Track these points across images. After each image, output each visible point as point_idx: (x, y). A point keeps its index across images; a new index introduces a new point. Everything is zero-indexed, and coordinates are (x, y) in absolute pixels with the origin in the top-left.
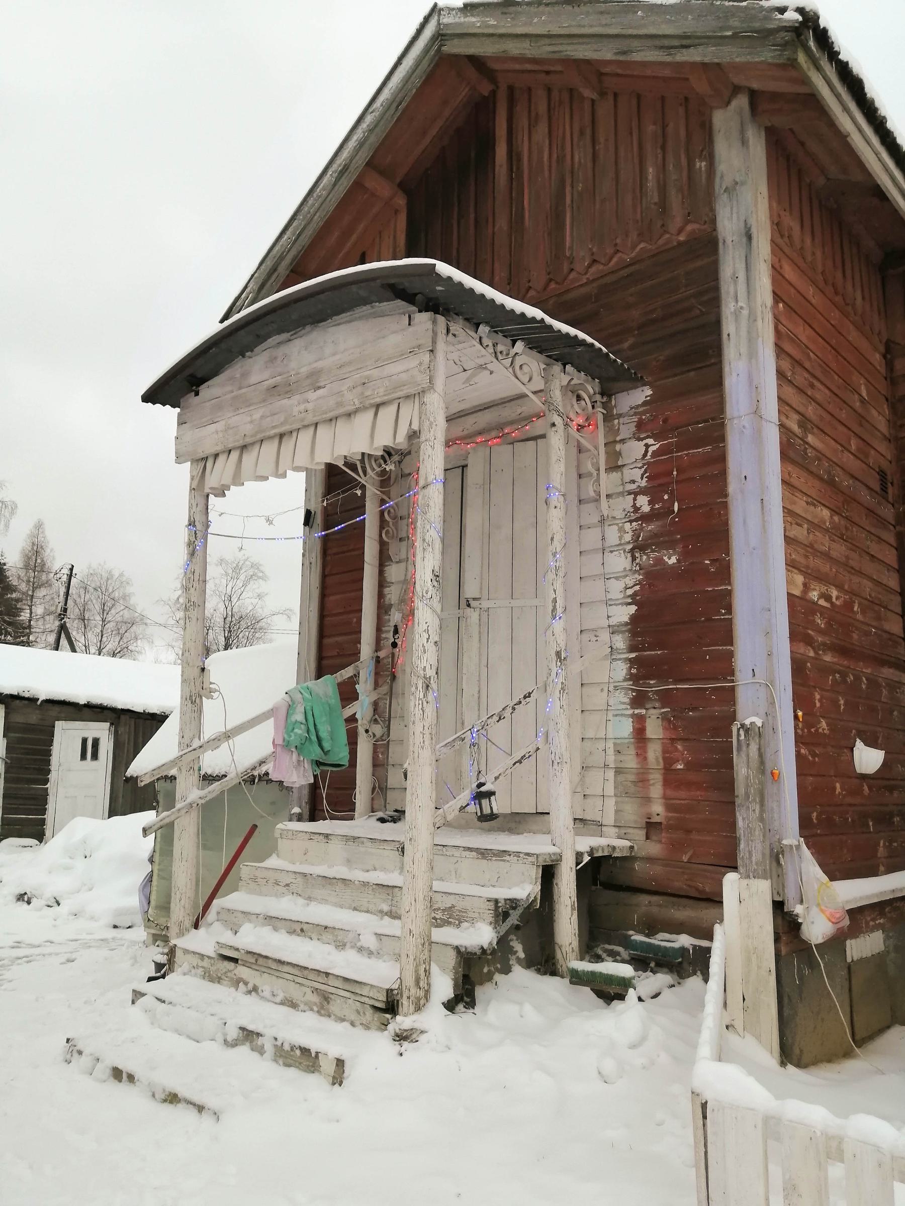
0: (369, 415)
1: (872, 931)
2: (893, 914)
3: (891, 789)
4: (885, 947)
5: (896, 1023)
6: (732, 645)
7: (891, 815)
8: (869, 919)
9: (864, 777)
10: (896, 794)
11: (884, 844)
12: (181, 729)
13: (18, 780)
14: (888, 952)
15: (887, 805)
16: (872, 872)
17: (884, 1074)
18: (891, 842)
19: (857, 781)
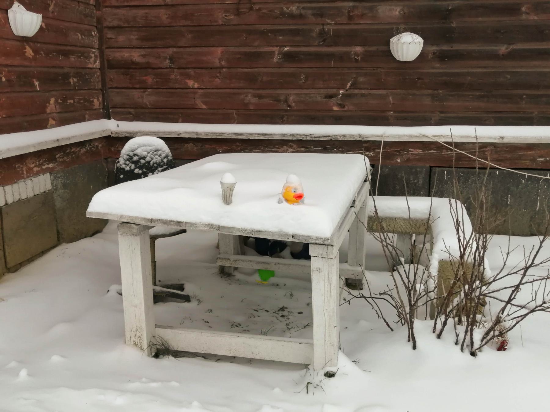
0: (545, 280)
1: (37, 174)
2: (65, 158)
3: (66, 54)
4: (53, 186)
5: (63, 242)
6: (377, 196)
7: (66, 76)
8: (32, 166)
9: (25, 40)
10: (72, 58)
11: (56, 101)
12: (96, 132)
13: (176, 149)
14: (56, 190)
15: (62, 68)
16: (41, 125)
17: (4, 300)
18: (65, 100)
19: (18, 43)
